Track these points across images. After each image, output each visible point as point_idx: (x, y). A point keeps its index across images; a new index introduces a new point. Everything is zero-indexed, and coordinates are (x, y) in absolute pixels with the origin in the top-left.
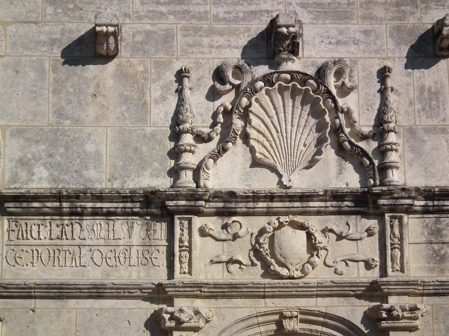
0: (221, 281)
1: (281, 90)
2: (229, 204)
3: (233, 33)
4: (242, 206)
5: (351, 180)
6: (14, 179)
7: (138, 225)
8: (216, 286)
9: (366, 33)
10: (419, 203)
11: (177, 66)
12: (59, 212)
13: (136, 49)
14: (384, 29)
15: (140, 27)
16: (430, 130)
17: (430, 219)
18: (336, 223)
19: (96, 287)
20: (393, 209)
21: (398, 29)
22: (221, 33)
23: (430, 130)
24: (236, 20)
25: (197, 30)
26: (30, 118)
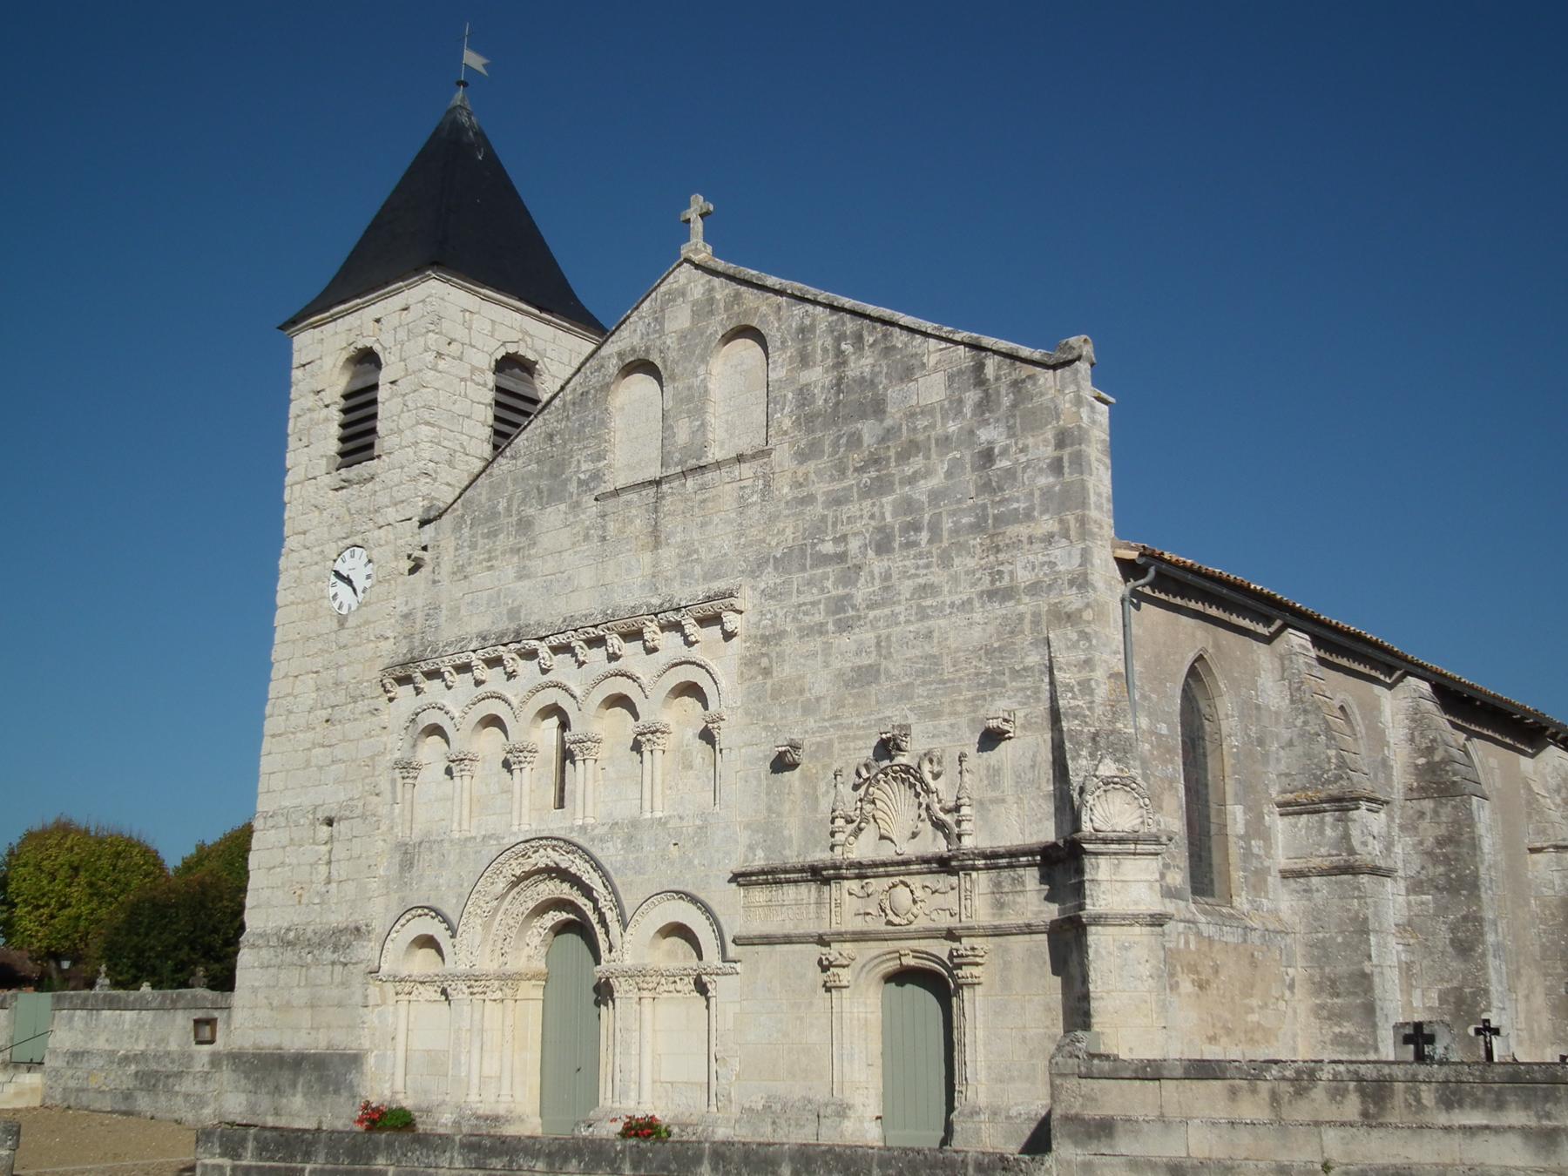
0: (793, 932)
1: (895, 779)
2: (862, 871)
3: (868, 737)
4: (869, 872)
5: (940, 846)
6: (746, 860)
7: (813, 886)
8: (854, 933)
9: (952, 726)
10: (980, 863)
11: (836, 767)
12: (766, 882)
13: (812, 756)
14: (963, 721)
15: (814, 740)
16: (992, 801)
17: (993, 873)
18: (930, 880)
19: (786, 936)
20: (963, 868)
21: (973, 720)
22: (860, 738)
23: (992, 801)
24: (870, 727)
25: (847, 737)
26: (1147, 746)
